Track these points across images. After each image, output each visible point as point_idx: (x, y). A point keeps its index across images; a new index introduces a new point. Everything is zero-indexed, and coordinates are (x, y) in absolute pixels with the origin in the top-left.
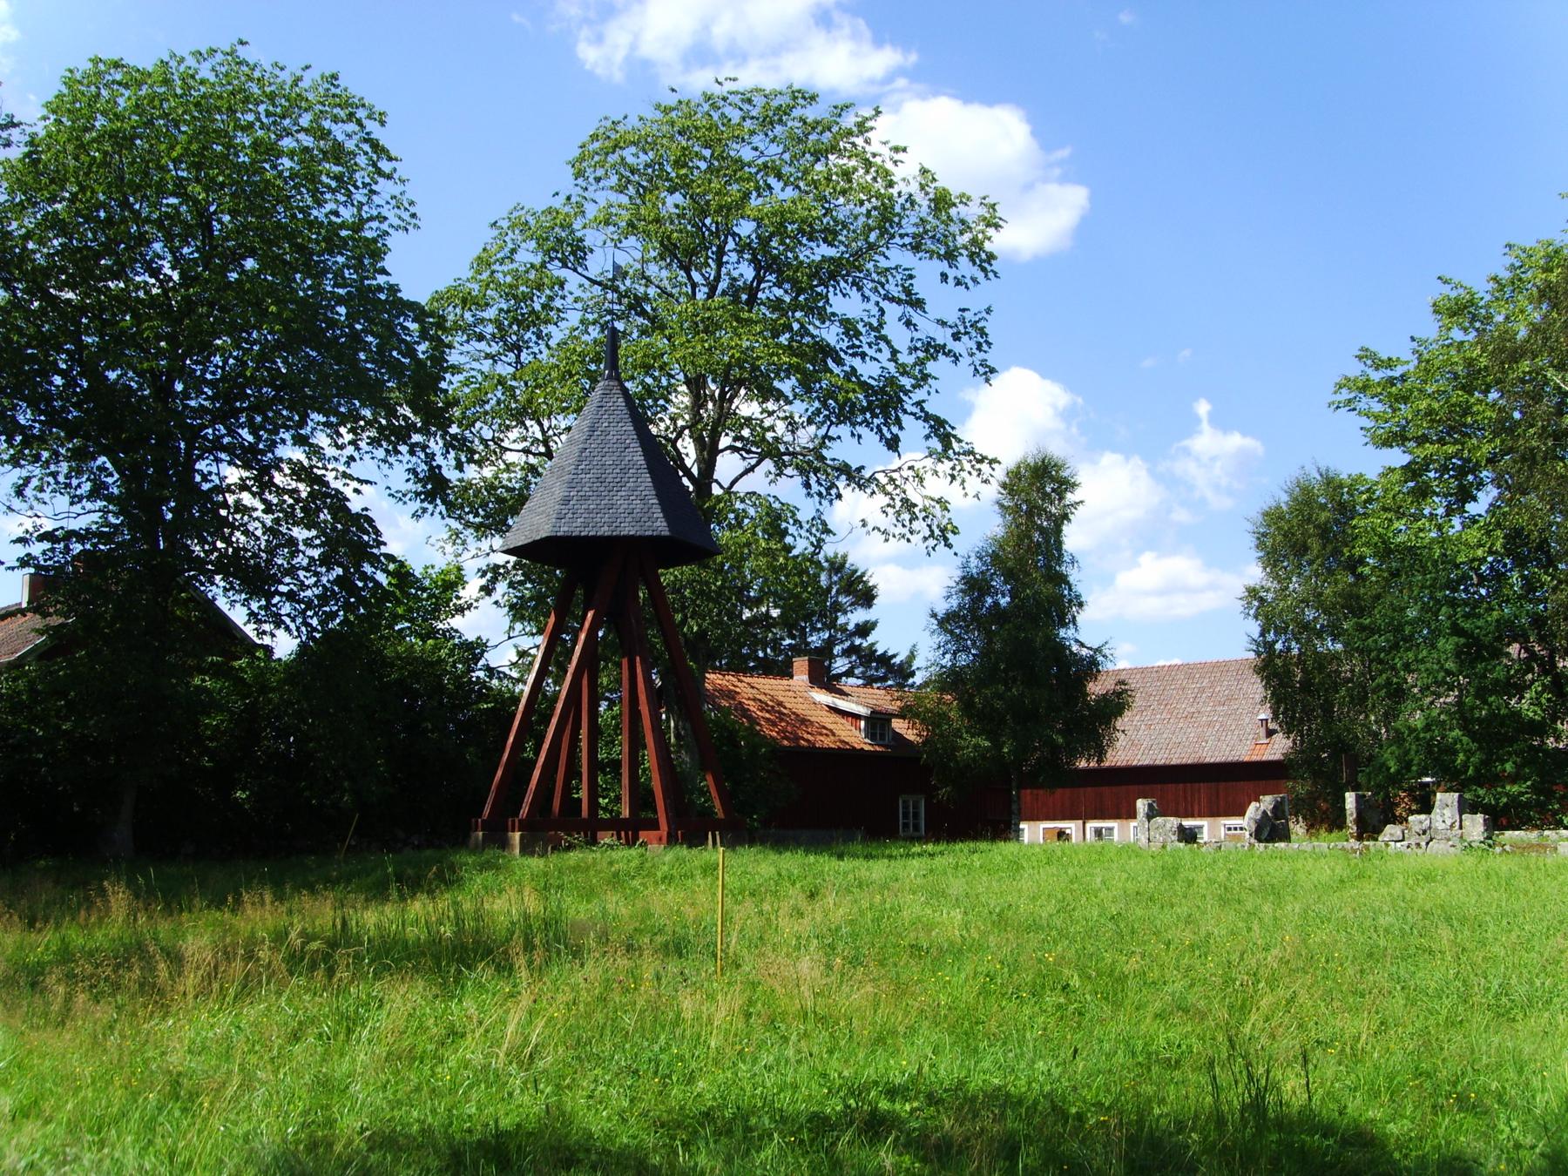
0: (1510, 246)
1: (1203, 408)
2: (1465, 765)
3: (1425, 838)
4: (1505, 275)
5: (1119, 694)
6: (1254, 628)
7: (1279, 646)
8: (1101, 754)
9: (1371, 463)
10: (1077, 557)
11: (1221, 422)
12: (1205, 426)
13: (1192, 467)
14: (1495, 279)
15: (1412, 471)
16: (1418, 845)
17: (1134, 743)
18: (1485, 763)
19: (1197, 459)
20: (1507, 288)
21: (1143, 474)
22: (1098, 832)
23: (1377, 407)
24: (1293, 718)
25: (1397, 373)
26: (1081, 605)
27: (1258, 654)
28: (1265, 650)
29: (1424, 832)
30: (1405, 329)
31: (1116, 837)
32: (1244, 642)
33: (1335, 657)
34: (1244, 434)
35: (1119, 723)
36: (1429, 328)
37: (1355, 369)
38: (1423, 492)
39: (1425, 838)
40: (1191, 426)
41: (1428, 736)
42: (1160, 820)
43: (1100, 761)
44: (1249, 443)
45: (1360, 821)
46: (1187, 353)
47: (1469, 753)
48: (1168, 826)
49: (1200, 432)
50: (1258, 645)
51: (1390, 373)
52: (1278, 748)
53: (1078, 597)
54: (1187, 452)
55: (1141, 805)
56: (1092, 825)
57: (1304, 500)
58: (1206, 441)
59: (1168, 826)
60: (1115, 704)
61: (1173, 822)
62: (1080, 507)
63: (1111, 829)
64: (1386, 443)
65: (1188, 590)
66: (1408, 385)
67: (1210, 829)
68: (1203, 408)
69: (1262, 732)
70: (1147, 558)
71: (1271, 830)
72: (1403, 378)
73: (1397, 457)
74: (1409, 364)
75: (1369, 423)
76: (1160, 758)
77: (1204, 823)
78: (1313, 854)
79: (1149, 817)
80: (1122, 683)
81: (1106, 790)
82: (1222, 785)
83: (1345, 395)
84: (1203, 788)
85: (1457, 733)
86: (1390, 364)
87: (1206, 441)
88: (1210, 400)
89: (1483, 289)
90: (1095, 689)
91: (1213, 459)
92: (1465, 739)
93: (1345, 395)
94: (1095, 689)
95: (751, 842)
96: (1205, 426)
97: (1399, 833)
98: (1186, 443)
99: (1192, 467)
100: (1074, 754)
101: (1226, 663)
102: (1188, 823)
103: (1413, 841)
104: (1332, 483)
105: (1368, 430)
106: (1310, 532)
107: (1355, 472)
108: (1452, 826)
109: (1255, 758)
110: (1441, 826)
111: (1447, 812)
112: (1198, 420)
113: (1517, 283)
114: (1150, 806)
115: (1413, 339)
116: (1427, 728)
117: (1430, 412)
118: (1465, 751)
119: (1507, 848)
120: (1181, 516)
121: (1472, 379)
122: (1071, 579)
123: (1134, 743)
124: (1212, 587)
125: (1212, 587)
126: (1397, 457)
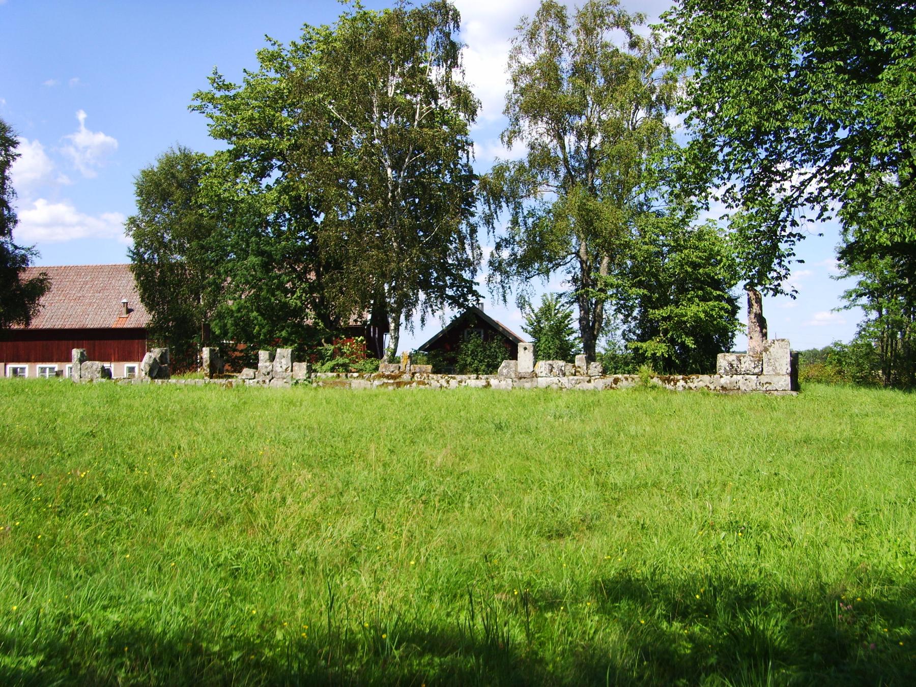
0: (307, 26)
1: (82, 116)
2: (259, 333)
3: (269, 377)
4: (301, 43)
5: (42, 281)
6: (131, 242)
7: (146, 256)
8: (28, 320)
9: (209, 146)
10: (17, 190)
11: (93, 126)
12: (83, 128)
13: (72, 150)
14: (294, 44)
15: (235, 154)
16: (264, 382)
17: (50, 314)
18: (271, 332)
19: (76, 148)
20: (302, 50)
21: (41, 152)
22: (15, 371)
23: (217, 114)
24: (153, 300)
25: (232, 93)
26: (16, 222)
27: (133, 259)
28: (136, 255)
29: (268, 374)
30: (241, 66)
31: (27, 374)
32: (125, 252)
33: (181, 265)
34: (107, 134)
35: (42, 300)
36: (255, 67)
37: (207, 87)
38: (239, 169)
39: (269, 377)
40: (74, 126)
41: (239, 315)
42: (88, 363)
43: (28, 324)
44: (109, 139)
45: (212, 366)
46: (76, 80)
47: (262, 326)
48: (95, 367)
49: (79, 132)
50: (134, 254)
51: (227, 93)
52: (141, 317)
53: (15, 216)
54: (70, 142)
55: (76, 353)
56: (11, 366)
57: (169, 164)
58: (83, 137)
59: (95, 367)
60: (39, 287)
61: (98, 365)
62: (18, 159)
63: (23, 369)
64: (222, 136)
65: (64, 225)
66: (238, 101)
67: (119, 369)
68: (82, 116)
69: (124, 310)
70: (40, 203)
71: (157, 372)
72: (234, 98)
73: (224, 146)
74: (240, 87)
75: (210, 121)
76: (58, 325)
77: (26, 366)
78: (194, 387)
79: (81, 361)
80: (45, 274)
81: (21, 344)
82: (97, 342)
83: (198, 103)
84: (113, 344)
85: (255, 314)
86: (228, 87)
87: (83, 137)
88: (86, 112)
89: (287, 51)
90: (25, 277)
91: (86, 148)
92: (260, 318)
93: (198, 103)
94: (25, 277)
95: (900, 389)
96: (83, 128)
97: (252, 374)
98: (69, 136)
99: (72, 150)
100: (10, 319)
101: (102, 267)
102: (107, 365)
103: (261, 379)
104: (187, 157)
105: (212, 126)
106: (170, 188)
107: (200, 152)
108: (286, 370)
109: (119, 326)
110: (279, 369)
111: (284, 361)
112: (78, 124)
113: (306, 50)
114: (82, 354)
115: (245, 71)
116: (239, 311)
117: (251, 119)
118: (259, 325)
119: (321, 384)
120: (64, 180)
121: (277, 99)
122: (10, 205)
123: (50, 314)
124: (81, 224)
125: (81, 224)
126: (224, 146)
